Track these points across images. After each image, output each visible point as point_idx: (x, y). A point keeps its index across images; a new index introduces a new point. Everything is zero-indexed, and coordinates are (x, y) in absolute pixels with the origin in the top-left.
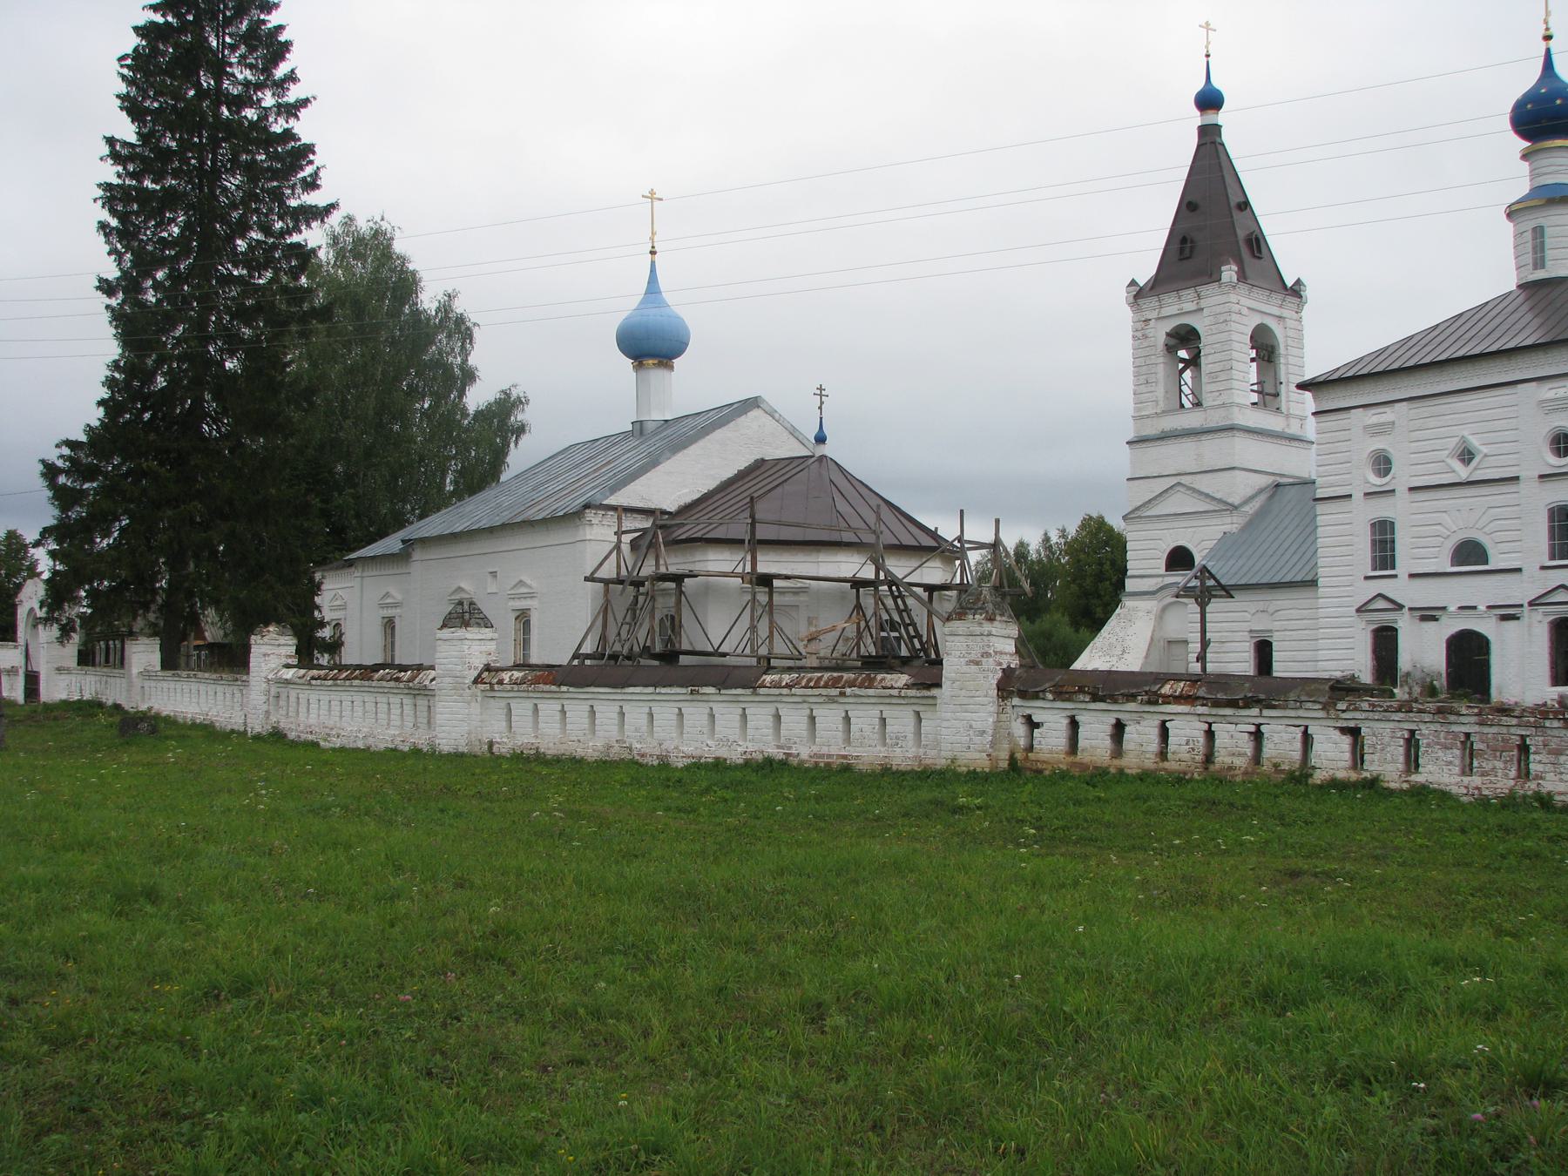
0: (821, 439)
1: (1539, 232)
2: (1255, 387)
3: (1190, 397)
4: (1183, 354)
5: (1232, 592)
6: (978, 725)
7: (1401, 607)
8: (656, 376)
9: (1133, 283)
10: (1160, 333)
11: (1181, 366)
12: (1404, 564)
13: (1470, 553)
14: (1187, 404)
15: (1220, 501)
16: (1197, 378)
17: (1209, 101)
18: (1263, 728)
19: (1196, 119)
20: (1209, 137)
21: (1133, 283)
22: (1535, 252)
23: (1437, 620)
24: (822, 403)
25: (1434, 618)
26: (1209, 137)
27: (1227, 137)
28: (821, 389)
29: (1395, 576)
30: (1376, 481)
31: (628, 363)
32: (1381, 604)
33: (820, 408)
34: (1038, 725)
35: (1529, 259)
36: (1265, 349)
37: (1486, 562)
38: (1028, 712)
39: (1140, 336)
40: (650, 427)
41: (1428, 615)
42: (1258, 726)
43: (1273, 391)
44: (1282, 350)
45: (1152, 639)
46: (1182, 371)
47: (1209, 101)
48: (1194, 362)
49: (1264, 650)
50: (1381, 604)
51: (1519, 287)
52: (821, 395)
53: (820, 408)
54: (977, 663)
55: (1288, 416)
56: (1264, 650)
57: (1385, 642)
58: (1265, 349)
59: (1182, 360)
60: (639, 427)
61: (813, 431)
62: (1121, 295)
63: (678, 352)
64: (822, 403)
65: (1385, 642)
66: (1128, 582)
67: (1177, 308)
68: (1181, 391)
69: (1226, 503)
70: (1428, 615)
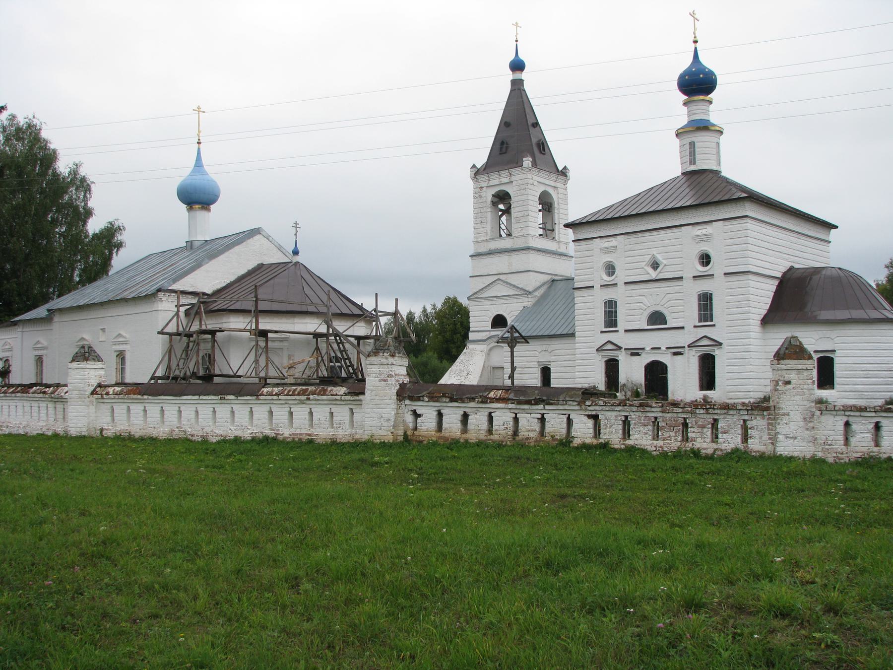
0: (296, 252)
1: (692, 145)
2: (541, 226)
3: (505, 231)
4: (501, 207)
5: (528, 340)
6: (386, 416)
7: (620, 348)
8: (200, 215)
9: (474, 166)
10: (489, 194)
11: (500, 213)
12: (622, 324)
13: (657, 318)
14: (504, 235)
15: (522, 289)
16: (509, 220)
17: (517, 66)
18: (545, 416)
19: (509, 76)
20: (517, 86)
21: (474, 166)
22: (690, 156)
23: (640, 355)
24: (297, 232)
25: (638, 354)
26: (517, 86)
27: (526, 86)
28: (296, 224)
29: (617, 331)
30: (607, 279)
31: (184, 207)
32: (610, 347)
33: (296, 235)
34: (419, 416)
35: (687, 159)
36: (547, 205)
37: (666, 324)
38: (414, 408)
39: (478, 196)
40: (196, 244)
41: (635, 352)
42: (543, 415)
43: (551, 228)
44: (556, 205)
45: (484, 366)
46: (501, 216)
47: (517, 66)
48: (507, 211)
49: (546, 372)
50: (610, 347)
51: (683, 174)
52: (296, 227)
53: (296, 235)
54: (385, 381)
55: (559, 242)
56: (546, 372)
57: (612, 367)
58: (547, 205)
59: (501, 210)
60: (190, 244)
61: (290, 249)
62: (467, 173)
63: (213, 200)
64: (297, 232)
65: (612, 367)
66: (470, 334)
67: (498, 181)
68: (500, 227)
69: (524, 290)
70: (635, 352)
